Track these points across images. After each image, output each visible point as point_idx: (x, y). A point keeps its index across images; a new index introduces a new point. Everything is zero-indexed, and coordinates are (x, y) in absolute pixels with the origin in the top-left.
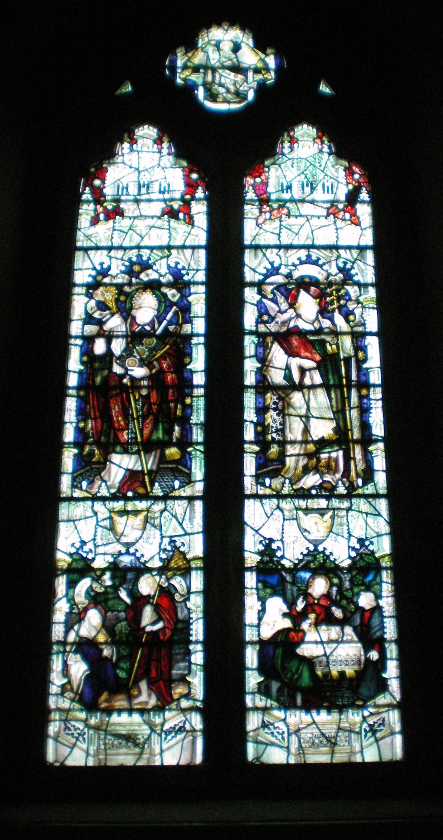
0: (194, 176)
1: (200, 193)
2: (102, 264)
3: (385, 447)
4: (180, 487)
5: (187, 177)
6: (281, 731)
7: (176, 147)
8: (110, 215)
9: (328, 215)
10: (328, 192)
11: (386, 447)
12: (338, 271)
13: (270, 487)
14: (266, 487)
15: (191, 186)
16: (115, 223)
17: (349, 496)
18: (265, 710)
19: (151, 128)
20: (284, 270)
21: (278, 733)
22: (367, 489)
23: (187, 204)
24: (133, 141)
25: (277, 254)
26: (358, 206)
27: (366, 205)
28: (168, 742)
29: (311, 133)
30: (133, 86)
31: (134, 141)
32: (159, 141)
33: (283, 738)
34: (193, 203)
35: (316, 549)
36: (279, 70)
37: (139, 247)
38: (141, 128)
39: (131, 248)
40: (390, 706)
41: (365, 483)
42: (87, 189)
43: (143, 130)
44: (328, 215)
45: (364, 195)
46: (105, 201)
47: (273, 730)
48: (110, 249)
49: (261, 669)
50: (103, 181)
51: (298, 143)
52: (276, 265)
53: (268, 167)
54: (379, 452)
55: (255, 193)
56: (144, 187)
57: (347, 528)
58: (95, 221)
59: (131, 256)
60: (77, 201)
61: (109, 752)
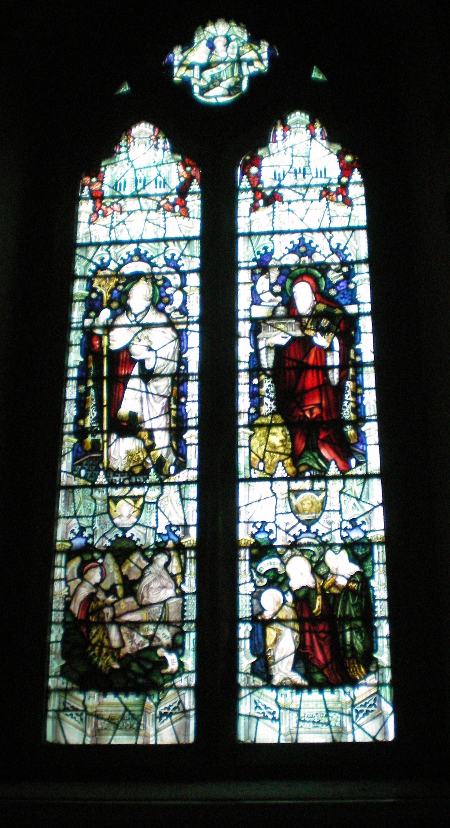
0: (349, 158)
1: (356, 176)
2: (265, 248)
7: (328, 132)
8: (270, 201)
9: (321, 198)
10: (160, 187)
12: (331, 253)
13: (264, 470)
16: (274, 208)
19: (148, 125)
24: (286, 127)
25: (107, 250)
26: (189, 198)
27: (358, 186)
29: (303, 119)
30: (130, 85)
31: (287, 128)
32: (310, 127)
36: (271, 59)
39: (131, 242)
42: (245, 177)
43: (295, 116)
44: (321, 198)
48: (272, 233)
50: (260, 167)
51: (291, 131)
52: (105, 261)
53: (105, 166)
55: (249, 181)
56: (300, 172)
57: (156, 514)
58: (254, 208)
60: (76, 200)
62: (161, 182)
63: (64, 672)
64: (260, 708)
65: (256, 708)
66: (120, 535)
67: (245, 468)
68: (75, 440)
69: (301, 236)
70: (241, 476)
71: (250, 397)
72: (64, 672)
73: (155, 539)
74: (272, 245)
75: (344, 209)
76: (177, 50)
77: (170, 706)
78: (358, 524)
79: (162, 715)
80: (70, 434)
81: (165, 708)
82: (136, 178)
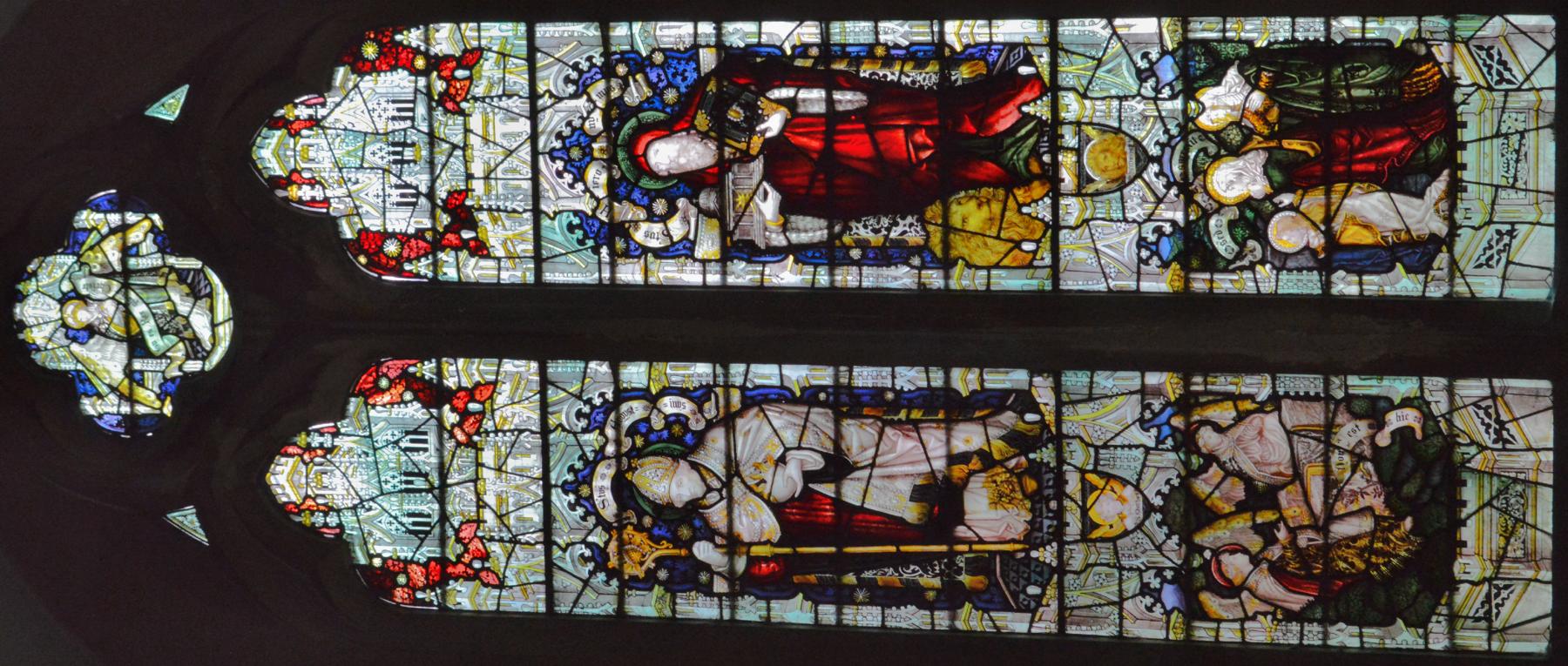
1: (413, 37)
3: (961, 366)
4: (1038, 411)
5: (372, 68)
6: (1496, 237)
8: (460, 212)
10: (425, 441)
11: (954, 17)
13: (1038, 242)
14: (1043, 594)
15: (395, 58)
17: (1059, 440)
18: (1453, 618)
20: (597, 538)
21: (1498, 242)
22: (1046, 404)
23: (436, 63)
28: (1512, 437)
30: (178, 507)
32: (292, 129)
33: (1506, 587)
34: (435, 50)
35: (1161, 510)
37: (547, 488)
38: (279, 491)
40: (1450, 391)
41: (1035, 408)
44: (462, 113)
45: (427, 369)
46: (434, 229)
47: (1494, 251)
49: (1385, 621)
53: (371, 557)
54: (965, 30)
55: (418, 258)
58: (479, 249)
59: (566, 504)
61: (1531, 186)
62: (399, 110)
63: (1420, 622)
64: (1491, 258)
65: (1490, 266)
66: (1159, 517)
69: (560, 490)
72: (1420, 622)
73: (1168, 450)
74: (565, 214)
76: (89, 406)
82: (401, 491)
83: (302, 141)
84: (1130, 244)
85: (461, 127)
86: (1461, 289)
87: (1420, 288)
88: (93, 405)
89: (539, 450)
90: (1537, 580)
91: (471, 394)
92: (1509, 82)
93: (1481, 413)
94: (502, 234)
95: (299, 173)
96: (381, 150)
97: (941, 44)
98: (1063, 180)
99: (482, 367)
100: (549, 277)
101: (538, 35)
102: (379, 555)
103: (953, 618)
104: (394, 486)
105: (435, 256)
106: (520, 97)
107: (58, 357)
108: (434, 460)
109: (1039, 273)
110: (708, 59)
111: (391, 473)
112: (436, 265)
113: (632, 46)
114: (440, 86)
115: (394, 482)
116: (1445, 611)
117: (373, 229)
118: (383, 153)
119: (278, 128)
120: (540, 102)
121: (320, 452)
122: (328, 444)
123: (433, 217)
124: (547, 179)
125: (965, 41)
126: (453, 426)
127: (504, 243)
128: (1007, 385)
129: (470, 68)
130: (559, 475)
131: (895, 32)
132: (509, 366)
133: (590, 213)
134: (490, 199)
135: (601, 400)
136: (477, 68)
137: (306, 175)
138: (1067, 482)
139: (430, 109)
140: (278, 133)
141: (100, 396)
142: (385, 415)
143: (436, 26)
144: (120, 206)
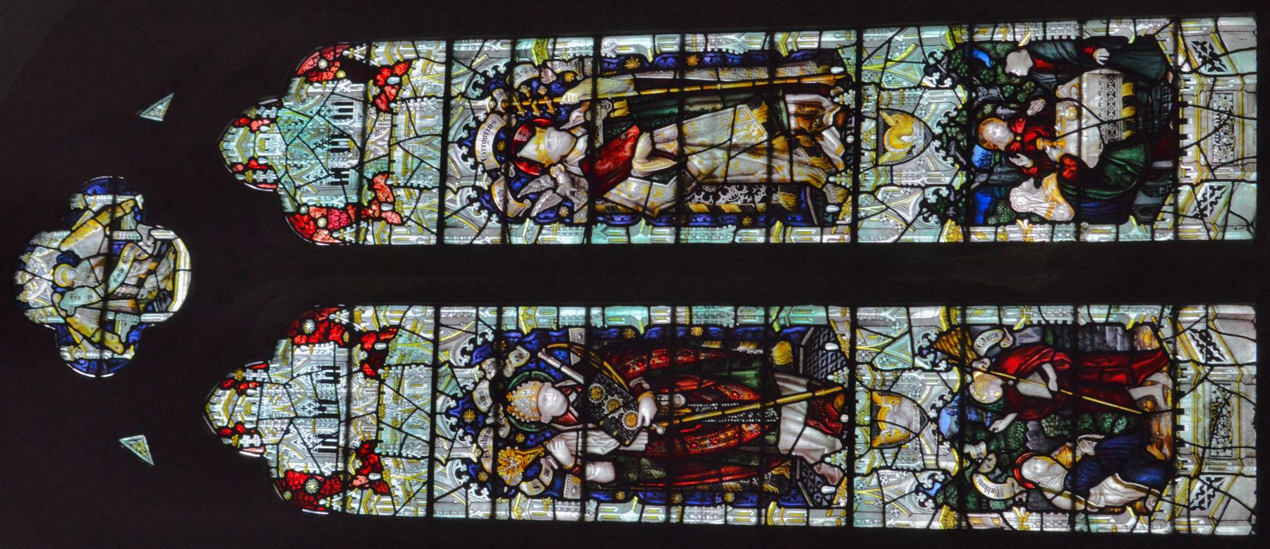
4: (843, 65)
5: (311, 340)
8: (369, 454)
10: (351, 110)
13: (840, 205)
22: (848, 59)
28: (1222, 355)
32: (241, 388)
33: (1220, 188)
45: (358, 53)
53: (299, 206)
55: (345, 228)
58: (382, 488)
59: (448, 426)
61: (1236, 443)
62: (341, 110)
63: (1149, 216)
64: (1203, 501)
65: (1203, 509)
66: (937, 143)
67: (835, 233)
68: (772, 505)
69: (456, 145)
70: (847, 238)
71: (721, 226)
72: (1149, 216)
73: (946, 88)
74: (466, 189)
75: (401, 342)
76: (67, 354)
77: (1198, 345)
78: (930, 501)
79: (1210, 356)
80: (768, 235)
81: (1201, 352)
82: (315, 417)
83: (261, 136)
84: (915, 204)
85: (389, 122)
86: (1182, 528)
87: (1149, 235)
88: (70, 352)
89: (430, 380)
90: (1243, 180)
91: (391, 69)
92: (1219, 69)
93: (1197, 336)
94: (401, 476)
95: (256, 160)
96: (310, 405)
97: (768, 326)
98: (857, 437)
99: (388, 314)
100: (438, 514)
101: (443, 316)
102: (305, 204)
103: (768, 235)
104: (310, 412)
105: (345, 494)
106: (437, 98)
107: (46, 316)
108: (358, 125)
109: (836, 512)
110: (576, 335)
111: (309, 402)
112: (344, 501)
113: (517, 326)
114: (375, 91)
115: (309, 407)
116: (1170, 209)
117: (298, 470)
118: (311, 409)
119: (228, 388)
120: (453, 102)
121: (266, 122)
122: (273, 116)
123: (359, 193)
124: (453, 161)
125: (790, 48)
126: (375, 97)
127: (403, 484)
128: (810, 321)
129: (387, 341)
130: (456, 132)
131: (733, 43)
132: (423, 47)
133: (475, 460)
134: (394, 448)
135: (494, 72)
136: (393, 342)
137: (262, 162)
138: (857, 401)
139: (365, 111)
140: (242, 130)
141: (76, 345)
142: (320, 90)
143: (363, 308)
144: (114, 189)
